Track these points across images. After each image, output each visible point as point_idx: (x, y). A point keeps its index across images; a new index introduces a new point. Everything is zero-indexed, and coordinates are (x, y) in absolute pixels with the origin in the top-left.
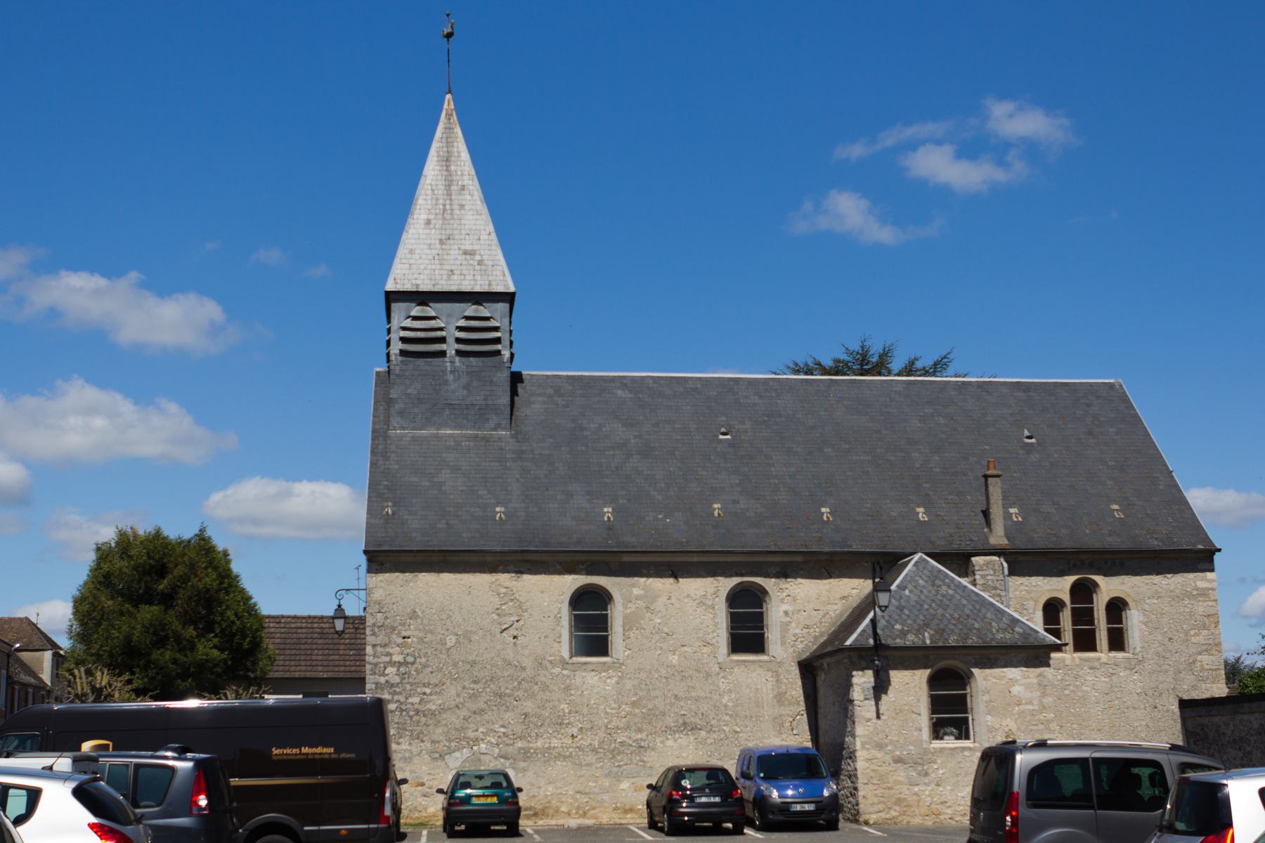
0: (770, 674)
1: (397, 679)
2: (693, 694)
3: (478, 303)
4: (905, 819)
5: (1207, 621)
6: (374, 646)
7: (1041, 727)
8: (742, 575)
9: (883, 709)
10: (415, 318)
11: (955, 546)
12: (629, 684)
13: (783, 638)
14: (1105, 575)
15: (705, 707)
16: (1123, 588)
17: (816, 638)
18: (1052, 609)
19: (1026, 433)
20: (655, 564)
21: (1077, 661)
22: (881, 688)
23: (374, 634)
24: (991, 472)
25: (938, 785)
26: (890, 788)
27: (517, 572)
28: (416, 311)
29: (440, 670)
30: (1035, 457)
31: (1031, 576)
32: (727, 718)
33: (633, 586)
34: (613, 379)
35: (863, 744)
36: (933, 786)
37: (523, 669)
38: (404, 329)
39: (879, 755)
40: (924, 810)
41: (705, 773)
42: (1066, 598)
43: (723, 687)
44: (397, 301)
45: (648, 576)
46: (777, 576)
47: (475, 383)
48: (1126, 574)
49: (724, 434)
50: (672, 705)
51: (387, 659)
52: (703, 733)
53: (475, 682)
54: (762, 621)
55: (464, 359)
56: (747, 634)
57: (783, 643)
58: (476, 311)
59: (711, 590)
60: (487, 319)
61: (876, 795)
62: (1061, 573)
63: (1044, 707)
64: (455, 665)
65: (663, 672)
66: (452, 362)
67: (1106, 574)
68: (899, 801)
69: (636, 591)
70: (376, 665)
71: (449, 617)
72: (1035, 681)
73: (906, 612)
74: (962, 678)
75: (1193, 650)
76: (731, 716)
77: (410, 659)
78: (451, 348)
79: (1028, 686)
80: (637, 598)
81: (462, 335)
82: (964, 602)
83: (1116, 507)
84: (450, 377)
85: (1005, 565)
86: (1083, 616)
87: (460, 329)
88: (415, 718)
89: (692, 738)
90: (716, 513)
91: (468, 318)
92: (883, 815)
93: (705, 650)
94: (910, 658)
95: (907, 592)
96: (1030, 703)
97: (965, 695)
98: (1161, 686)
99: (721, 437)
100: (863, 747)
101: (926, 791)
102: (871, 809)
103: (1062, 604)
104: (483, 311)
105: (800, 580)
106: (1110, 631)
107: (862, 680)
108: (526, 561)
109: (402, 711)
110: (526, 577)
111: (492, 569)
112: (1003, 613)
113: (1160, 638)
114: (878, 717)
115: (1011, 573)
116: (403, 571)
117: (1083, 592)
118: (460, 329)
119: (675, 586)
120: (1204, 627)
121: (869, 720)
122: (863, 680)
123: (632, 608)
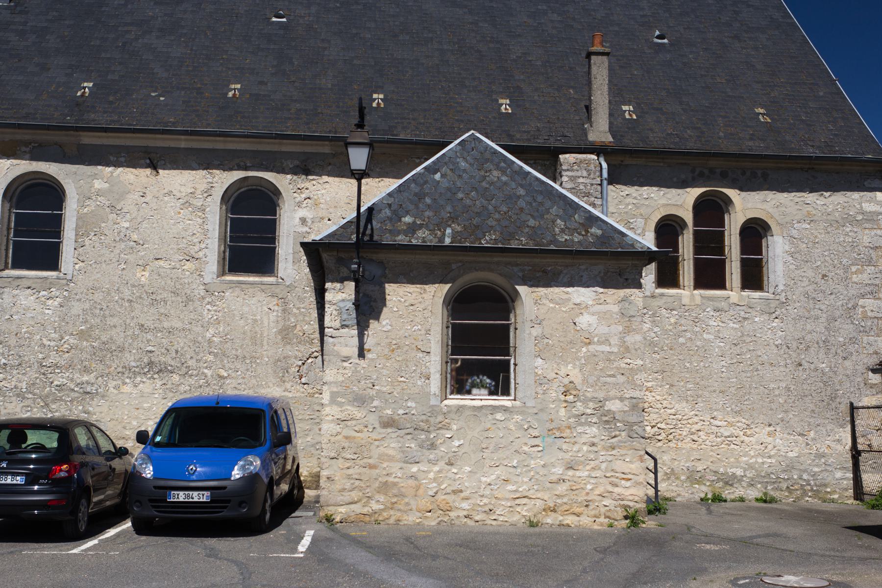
0: (275, 301)
2: (166, 324)
4: (394, 515)
5: (873, 254)
7: (621, 379)
8: (246, 169)
9: (369, 343)
11: (540, 142)
12: (77, 308)
14: (741, 190)
15: (180, 343)
16: (765, 206)
18: (668, 229)
19: (657, 33)
20: (128, 150)
21: (698, 300)
22: (367, 309)
25: (450, 464)
26: (372, 467)
32: (211, 358)
33: (95, 176)
35: (334, 396)
36: (442, 464)
39: (358, 413)
40: (425, 503)
42: (688, 217)
43: (207, 316)
45: (117, 165)
46: (295, 171)
48: (770, 189)
50: (135, 337)
52: (176, 378)
59: (203, 186)
61: (349, 477)
62: (683, 184)
63: (627, 349)
65: (127, 293)
67: (744, 187)
68: (385, 487)
69: (98, 184)
72: (616, 308)
73: (428, 200)
74: (506, 302)
75: (853, 292)
76: (216, 355)
79: (603, 317)
80: (99, 193)
82: (522, 192)
83: (762, 111)
85: (605, 165)
86: (710, 243)
89: (159, 383)
90: (230, 94)
92: (357, 508)
93: (189, 266)
94: (419, 266)
95: (437, 176)
96: (607, 342)
97: (507, 327)
98: (808, 337)
99: (274, 19)
100: (333, 401)
101: (429, 472)
102: (340, 499)
103: (682, 224)
105: (325, 178)
106: (744, 262)
112: (577, 207)
113: (810, 273)
114: (361, 354)
117: (711, 211)
119: (153, 179)
120: (870, 262)
121: (346, 359)
122: (341, 296)
123: (91, 206)
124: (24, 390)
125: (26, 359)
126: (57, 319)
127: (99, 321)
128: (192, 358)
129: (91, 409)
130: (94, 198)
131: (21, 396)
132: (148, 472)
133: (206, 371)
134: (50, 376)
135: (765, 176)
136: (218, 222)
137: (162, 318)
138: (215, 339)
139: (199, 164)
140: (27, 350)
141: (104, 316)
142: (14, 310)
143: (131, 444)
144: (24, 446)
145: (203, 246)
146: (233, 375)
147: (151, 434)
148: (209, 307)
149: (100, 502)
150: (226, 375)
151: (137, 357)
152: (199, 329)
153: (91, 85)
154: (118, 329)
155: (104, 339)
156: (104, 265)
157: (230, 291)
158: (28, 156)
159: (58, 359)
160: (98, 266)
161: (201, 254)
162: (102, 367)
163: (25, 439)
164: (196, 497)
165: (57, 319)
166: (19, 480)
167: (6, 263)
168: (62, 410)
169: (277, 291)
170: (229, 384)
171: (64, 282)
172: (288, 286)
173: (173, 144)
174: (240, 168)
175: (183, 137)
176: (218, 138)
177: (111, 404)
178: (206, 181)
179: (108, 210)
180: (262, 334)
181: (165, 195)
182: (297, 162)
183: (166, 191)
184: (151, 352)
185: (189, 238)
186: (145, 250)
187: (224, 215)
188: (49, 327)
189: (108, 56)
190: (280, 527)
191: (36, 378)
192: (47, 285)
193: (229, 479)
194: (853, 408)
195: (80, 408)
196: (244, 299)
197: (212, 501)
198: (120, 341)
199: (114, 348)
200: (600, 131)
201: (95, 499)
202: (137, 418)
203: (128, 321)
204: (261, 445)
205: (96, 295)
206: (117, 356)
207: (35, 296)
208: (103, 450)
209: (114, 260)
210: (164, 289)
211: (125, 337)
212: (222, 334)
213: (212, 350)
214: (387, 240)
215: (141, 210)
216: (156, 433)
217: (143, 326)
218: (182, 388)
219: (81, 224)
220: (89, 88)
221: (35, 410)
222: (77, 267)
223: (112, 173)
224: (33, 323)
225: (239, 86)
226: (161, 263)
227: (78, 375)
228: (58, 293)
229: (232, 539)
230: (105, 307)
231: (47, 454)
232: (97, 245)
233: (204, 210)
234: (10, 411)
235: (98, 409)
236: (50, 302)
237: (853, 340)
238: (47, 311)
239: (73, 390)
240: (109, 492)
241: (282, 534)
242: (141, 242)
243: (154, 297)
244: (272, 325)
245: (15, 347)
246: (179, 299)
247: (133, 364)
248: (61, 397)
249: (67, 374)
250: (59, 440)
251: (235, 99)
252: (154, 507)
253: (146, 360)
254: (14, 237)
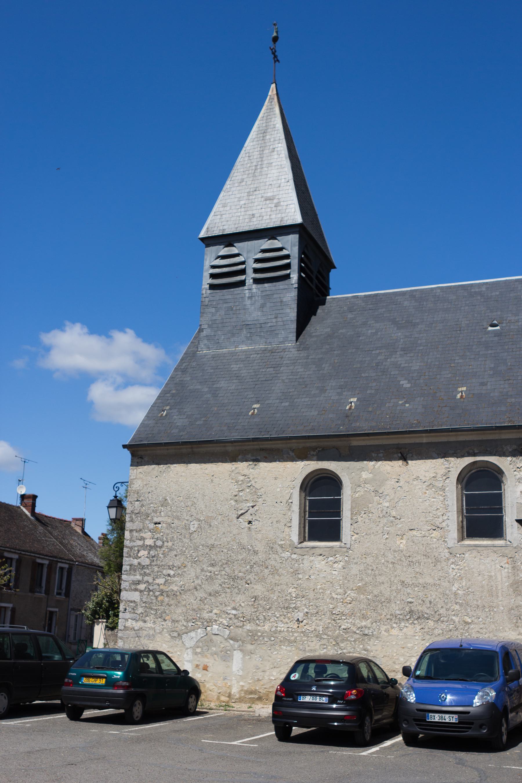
0: (505, 560)
2: (421, 581)
6: (131, 531)
8: (474, 455)
12: (355, 570)
15: (433, 595)
32: (457, 607)
33: (362, 469)
45: (377, 459)
50: (398, 591)
52: (431, 623)
59: (442, 471)
65: (390, 557)
69: (365, 475)
76: (461, 605)
77: (159, 543)
88: (160, 598)
89: (418, 627)
93: (435, 534)
99: (490, 328)
108: (262, 450)
109: (150, 591)
116: (158, 464)
119: (404, 469)
124: (321, 632)
125: (321, 608)
126: (341, 578)
127: (371, 579)
128: (442, 607)
129: (369, 647)
130: (362, 485)
131: (319, 636)
132: (412, 698)
133: (454, 618)
134: (338, 621)
136: (455, 498)
137: (418, 576)
138: (459, 592)
139: (438, 454)
140: (321, 601)
141: (375, 575)
142: (311, 572)
143: (400, 676)
144: (325, 675)
145: (445, 518)
146: (476, 621)
147: (413, 668)
148: (453, 566)
149: (378, 721)
150: (470, 621)
151: (401, 607)
152: (446, 584)
153: (355, 400)
154: (386, 585)
155: (376, 593)
156: (372, 536)
157: (469, 552)
158: (315, 458)
159: (344, 609)
160: (368, 537)
161: (444, 524)
162: (375, 615)
163: (325, 671)
164: (448, 718)
165: (341, 578)
166: (324, 700)
167: (305, 537)
168: (349, 648)
169: (507, 551)
170: (473, 629)
171: (345, 550)
172: (515, 548)
173: (418, 441)
174: (470, 455)
175: (424, 435)
176: (451, 433)
177: (384, 644)
178: (444, 467)
179: (373, 494)
180: (497, 588)
181: (414, 480)
182: (515, 447)
183: (414, 477)
184: (411, 603)
185: (434, 512)
186: (402, 523)
187: (460, 492)
188: (336, 584)
189: (367, 375)
190: (516, 747)
191: (329, 623)
192: (334, 553)
193: (471, 705)
195: (361, 646)
196: (480, 559)
197: (459, 723)
198: (387, 594)
199: (383, 600)
201: (376, 718)
202: (403, 655)
203: (392, 579)
204: (496, 680)
205: (368, 559)
206: (386, 606)
207: (325, 561)
208: (380, 681)
209: (380, 532)
210: (418, 553)
211: (391, 591)
212: (465, 588)
213: (458, 601)
215: (397, 492)
216: (417, 667)
217: (403, 582)
218: (436, 632)
219: (354, 505)
220: (354, 402)
221: (329, 647)
222: (353, 538)
223: (374, 466)
224: (325, 582)
225: (464, 389)
226: (414, 532)
227: (358, 621)
228: (341, 558)
229: (477, 754)
230: (375, 568)
231: (342, 682)
232: (367, 521)
233: (444, 490)
234: (312, 648)
235: (374, 648)
236: (336, 565)
238: (334, 572)
239: (355, 632)
240: (385, 713)
241: (517, 753)
242: (399, 517)
243: (410, 559)
244: (504, 580)
245: (313, 599)
246: (429, 560)
247: (398, 612)
248: (347, 638)
249: (351, 620)
250: (349, 673)
251: (462, 400)
252: (417, 725)
253: (407, 609)
254: (309, 517)
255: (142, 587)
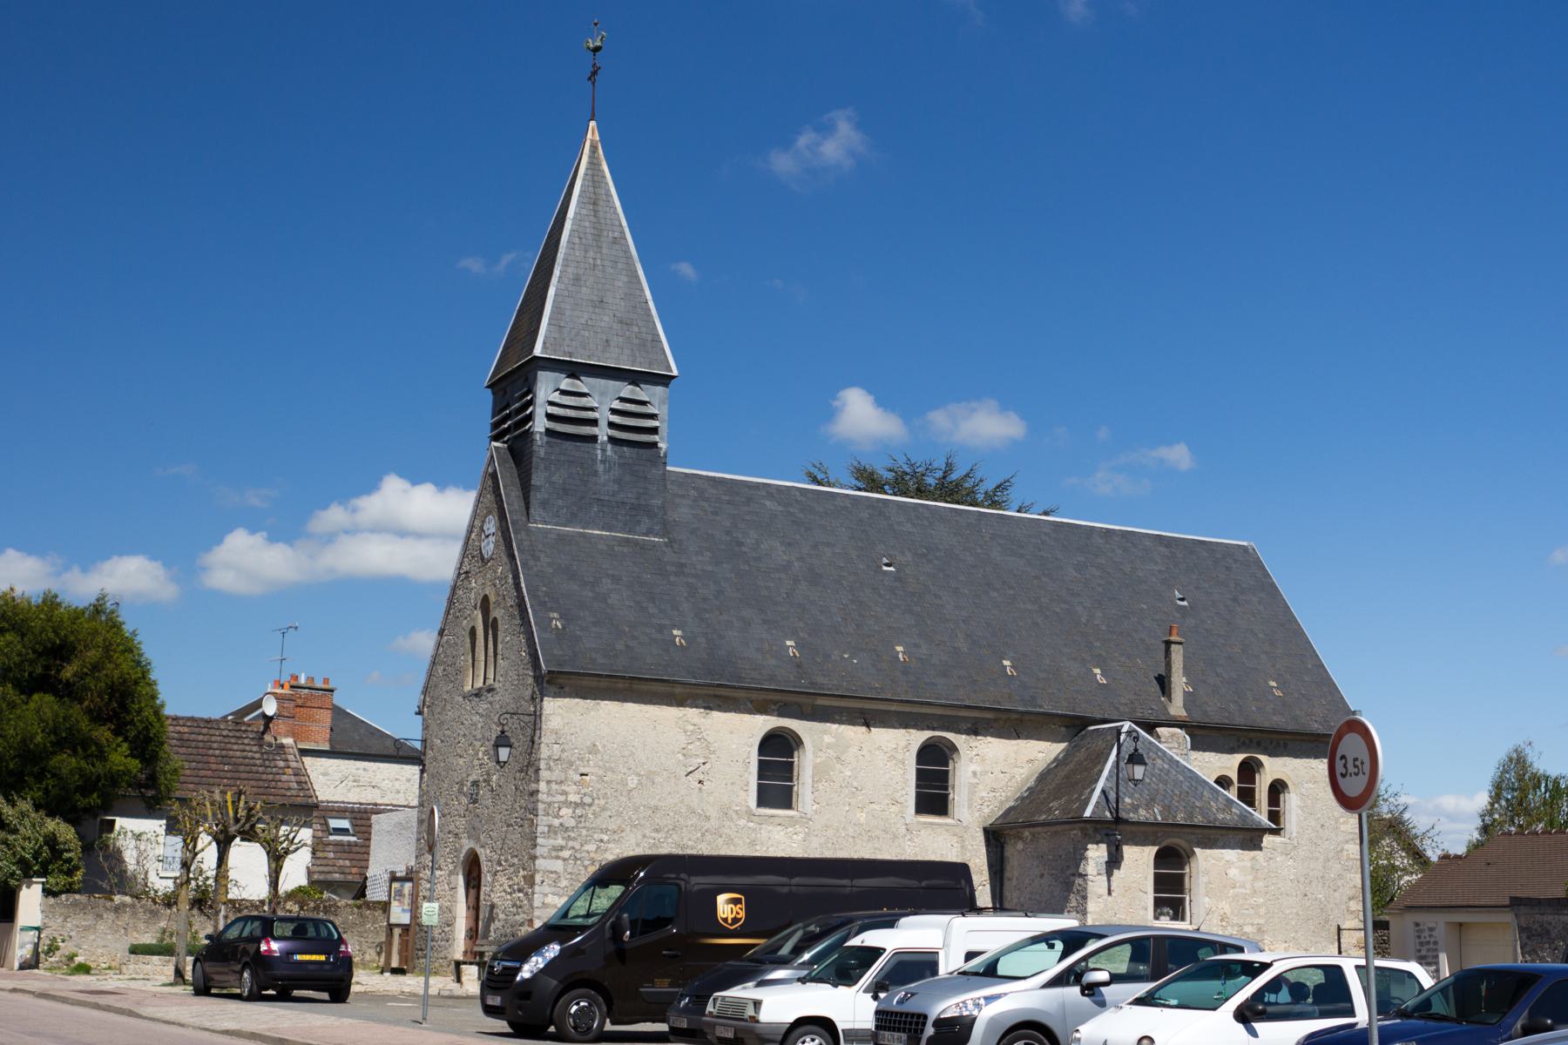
1: (572, 823)
3: (635, 383)
6: (549, 782)
10: (564, 393)
13: (970, 800)
17: (1002, 803)
20: (849, 710)
22: (1114, 862)
23: (549, 769)
24: (1173, 638)
27: (705, 708)
28: (566, 383)
29: (619, 814)
30: (1191, 622)
31: (1205, 750)
33: (825, 732)
34: (758, 486)
37: (708, 818)
38: (551, 403)
41: (291, 926)
42: (1234, 776)
44: (544, 369)
45: (840, 722)
47: (628, 478)
49: (888, 565)
51: (562, 798)
53: (657, 831)
54: (946, 780)
55: (617, 448)
56: (933, 796)
57: (970, 807)
58: (633, 392)
60: (643, 403)
62: (1232, 751)
64: (636, 810)
65: (851, 831)
66: (604, 451)
69: (827, 739)
70: (549, 804)
71: (632, 754)
77: (587, 800)
78: (602, 433)
81: (616, 419)
84: (600, 468)
87: (614, 411)
91: (622, 400)
93: (894, 809)
94: (1142, 833)
96: (1243, 886)
97: (1182, 876)
104: (641, 393)
105: (990, 739)
107: (1097, 854)
109: (576, 859)
110: (716, 714)
111: (680, 702)
113: (1313, 823)
114: (1110, 893)
115: (1193, 748)
116: (584, 698)
117: (1248, 771)
118: (614, 411)
135: (1285, 745)
174: (929, 728)
194: (1339, 929)
200: (1177, 708)
214: (1132, 816)
237: (1340, 876)
255: (566, 854)
